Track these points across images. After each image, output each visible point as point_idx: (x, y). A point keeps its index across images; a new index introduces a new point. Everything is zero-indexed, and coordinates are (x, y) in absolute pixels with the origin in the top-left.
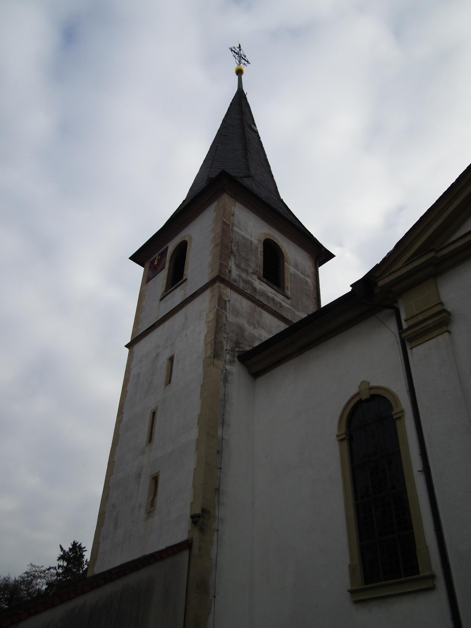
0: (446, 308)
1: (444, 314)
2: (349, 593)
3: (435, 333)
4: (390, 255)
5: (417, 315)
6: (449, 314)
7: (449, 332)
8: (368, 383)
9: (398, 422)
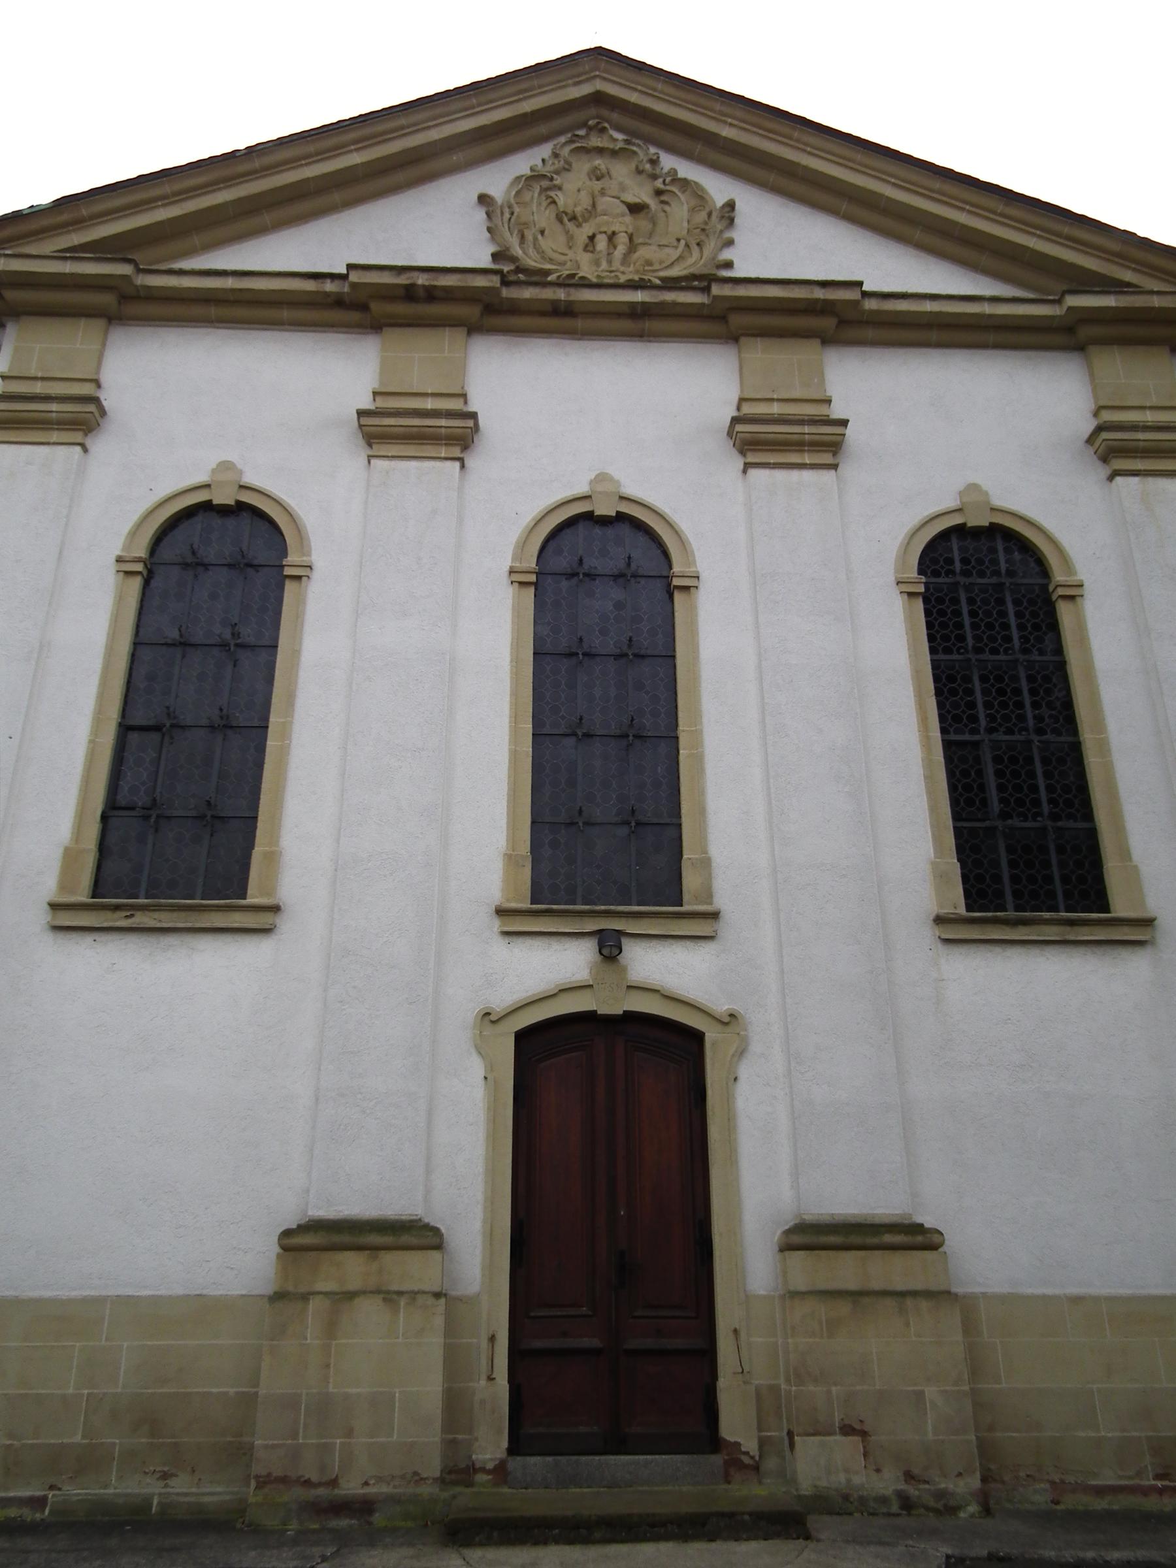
0: (102, 399)
1: (92, 408)
2: (47, 907)
3: (55, 436)
4: (35, 213)
5: (35, 379)
6: (103, 412)
7: (85, 450)
8: (241, 472)
9: (289, 586)
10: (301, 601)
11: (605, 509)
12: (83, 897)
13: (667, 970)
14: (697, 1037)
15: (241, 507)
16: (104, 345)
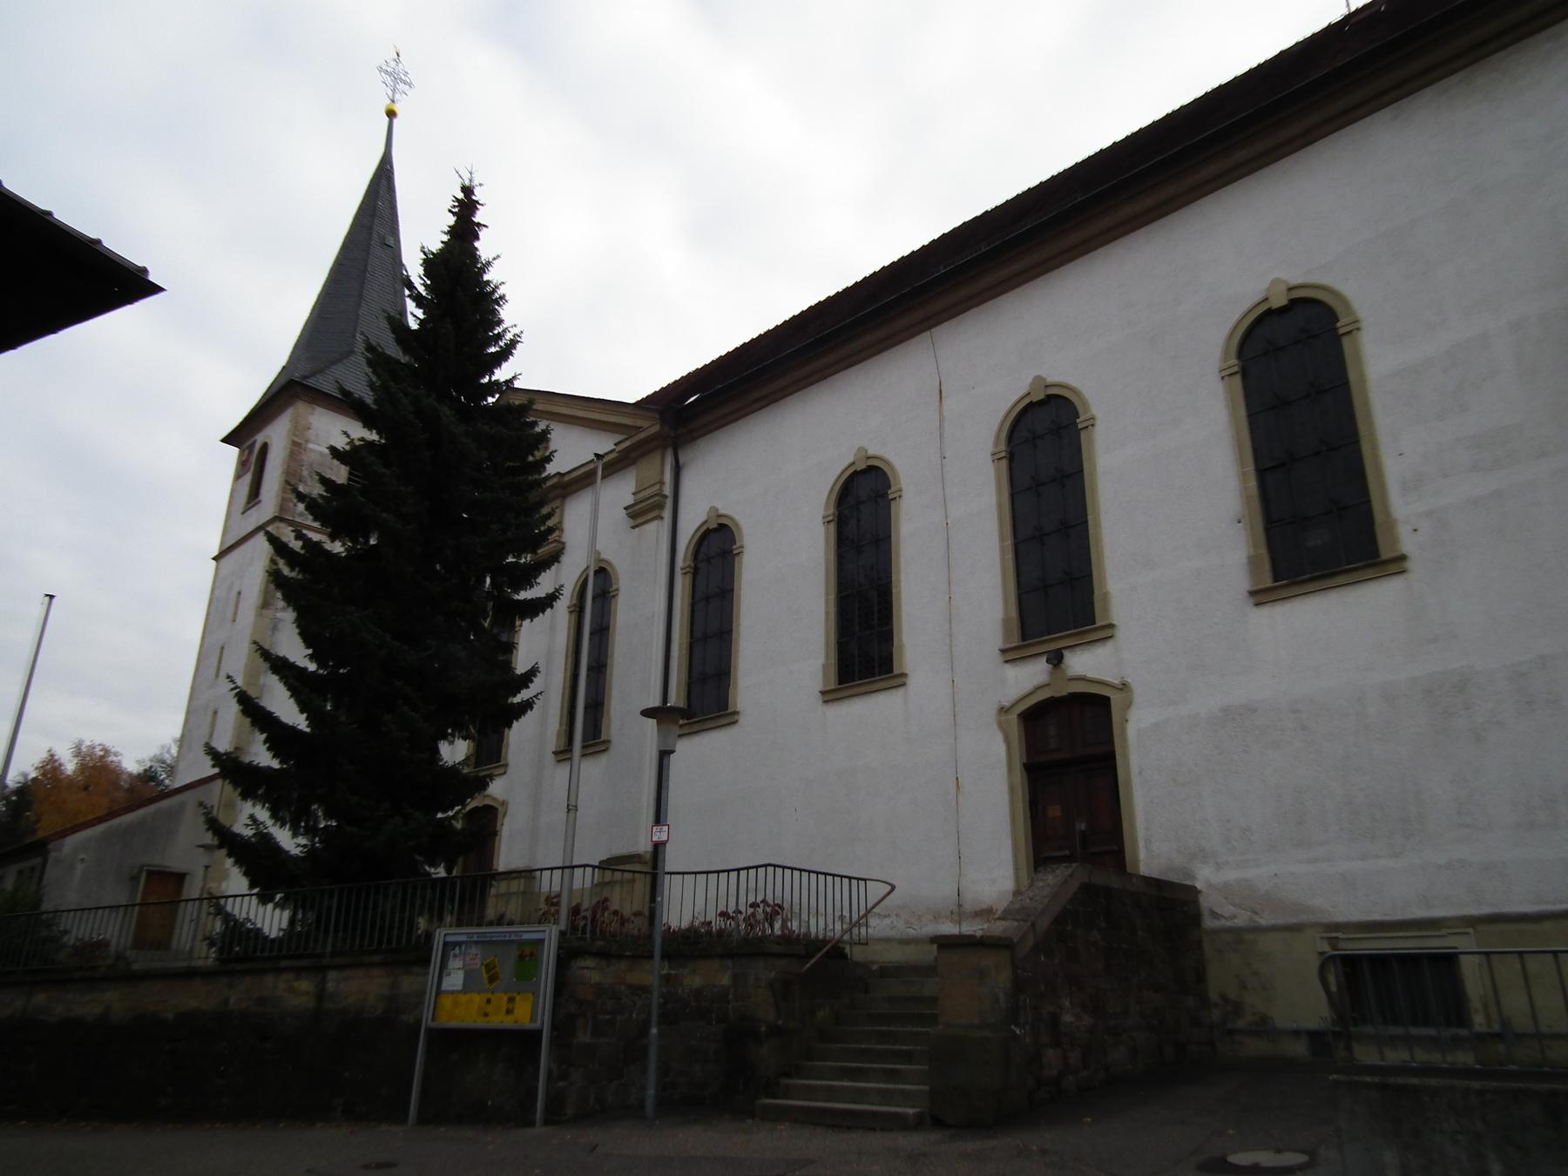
10: (1091, 442)
11: (1279, 301)
12: (1269, 583)
13: (1088, 664)
14: (1107, 699)
15: (1050, 397)
16: (677, 470)
